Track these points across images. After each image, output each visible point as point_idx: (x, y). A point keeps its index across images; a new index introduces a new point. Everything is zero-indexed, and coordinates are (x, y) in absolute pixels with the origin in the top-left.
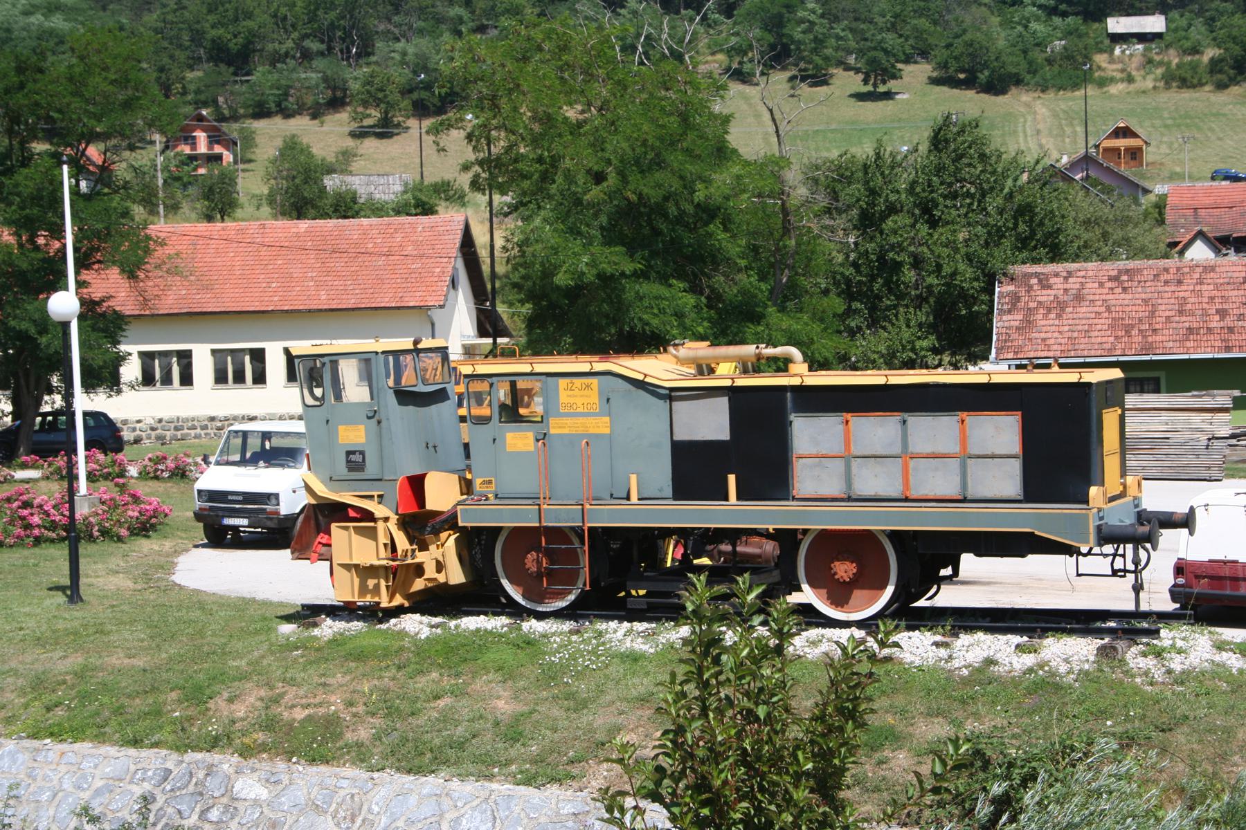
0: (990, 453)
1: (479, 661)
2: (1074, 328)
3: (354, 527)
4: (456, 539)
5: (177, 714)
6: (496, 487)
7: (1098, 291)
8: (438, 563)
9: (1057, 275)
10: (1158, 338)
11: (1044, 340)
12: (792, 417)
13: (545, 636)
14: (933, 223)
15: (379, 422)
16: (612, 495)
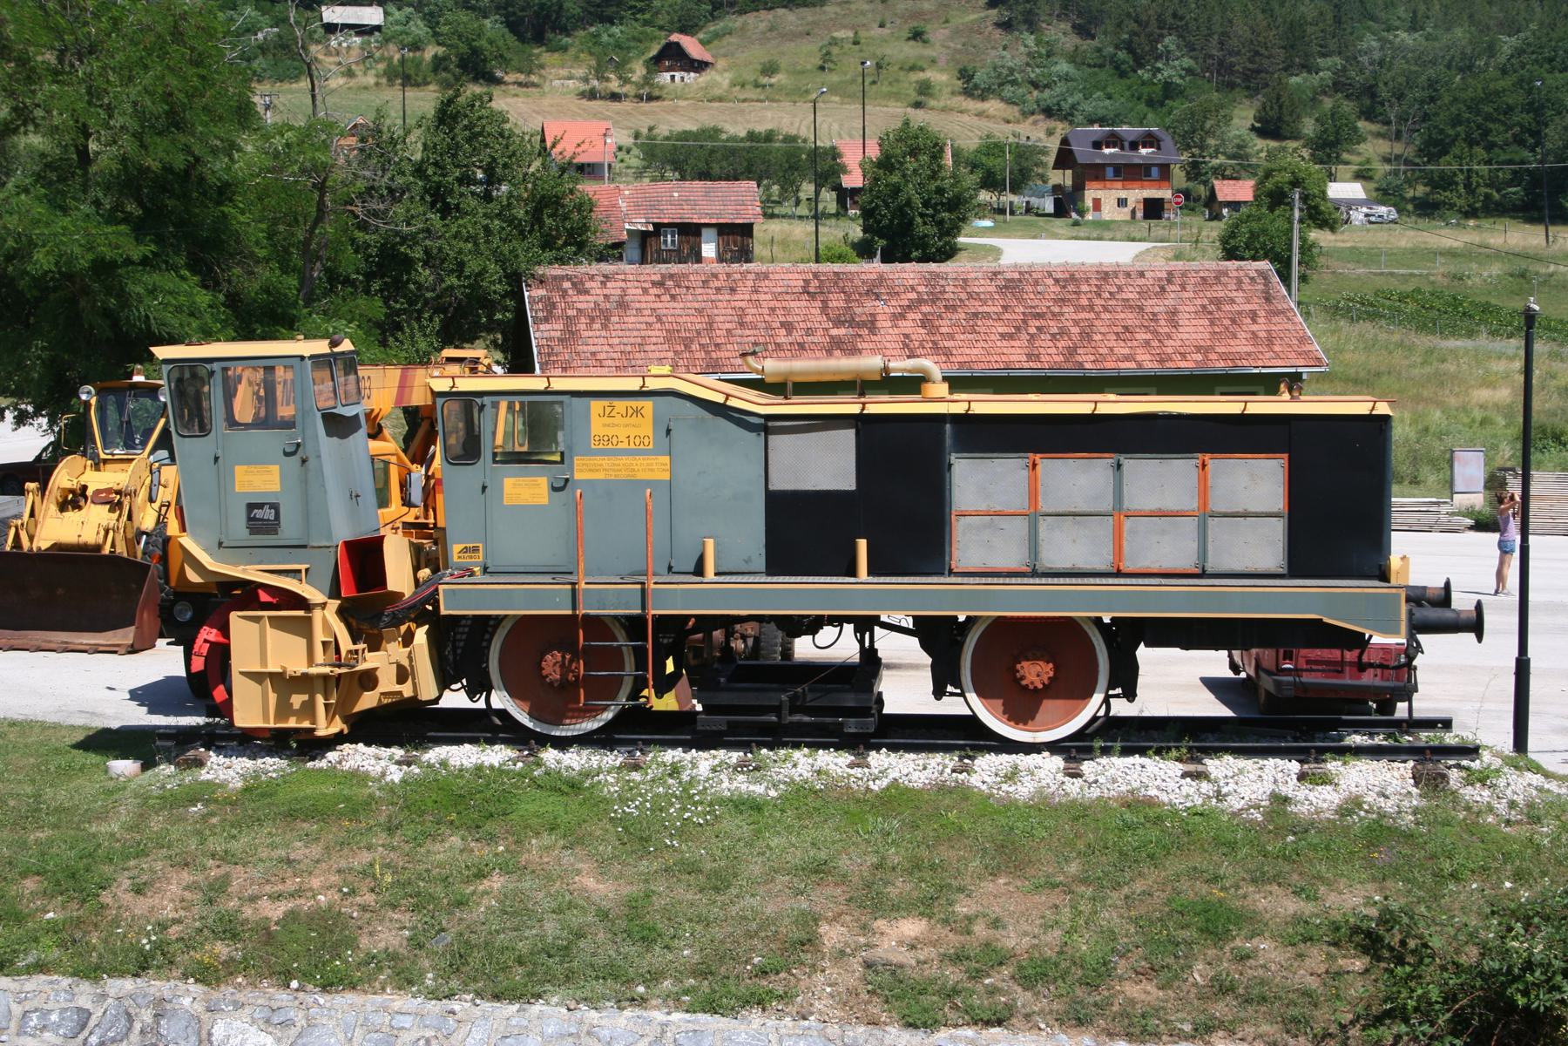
0: (1240, 510)
1: (512, 816)
2: (625, 341)
3: (269, 618)
4: (427, 633)
5: (51, 915)
6: (486, 556)
7: (643, 299)
8: (400, 668)
9: (592, 278)
10: (721, 355)
11: (593, 354)
12: (953, 457)
13: (587, 774)
14: (445, 211)
15: (304, 461)
16: (670, 568)
